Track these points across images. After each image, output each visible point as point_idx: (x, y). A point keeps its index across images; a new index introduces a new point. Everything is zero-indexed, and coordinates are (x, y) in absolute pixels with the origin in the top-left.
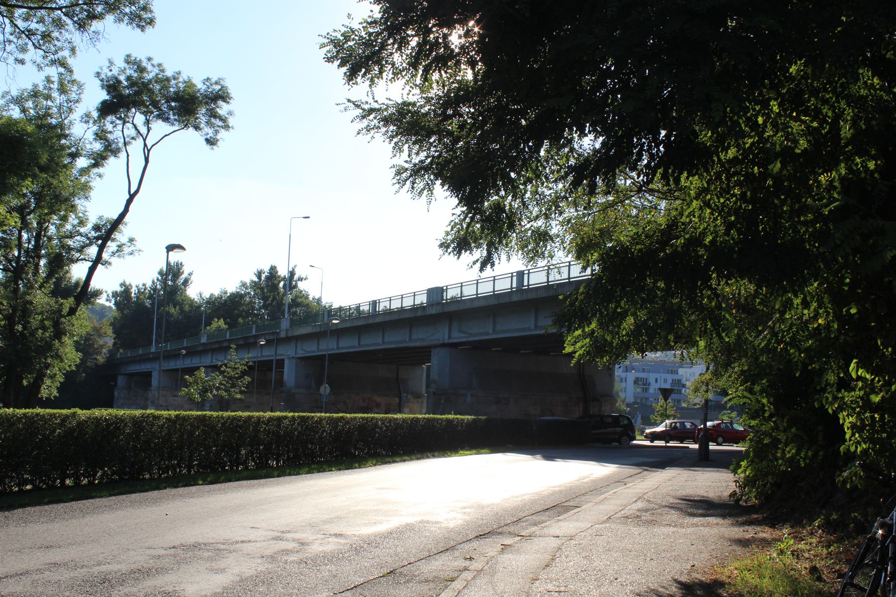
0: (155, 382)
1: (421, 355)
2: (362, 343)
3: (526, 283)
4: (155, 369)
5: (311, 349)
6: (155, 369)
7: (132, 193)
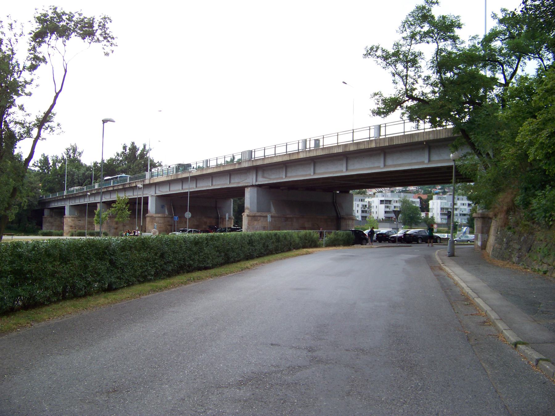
1: (239, 192)
2: (171, 189)
3: (253, 157)
4: (67, 205)
5: (165, 191)
6: (67, 205)
7: (57, 92)
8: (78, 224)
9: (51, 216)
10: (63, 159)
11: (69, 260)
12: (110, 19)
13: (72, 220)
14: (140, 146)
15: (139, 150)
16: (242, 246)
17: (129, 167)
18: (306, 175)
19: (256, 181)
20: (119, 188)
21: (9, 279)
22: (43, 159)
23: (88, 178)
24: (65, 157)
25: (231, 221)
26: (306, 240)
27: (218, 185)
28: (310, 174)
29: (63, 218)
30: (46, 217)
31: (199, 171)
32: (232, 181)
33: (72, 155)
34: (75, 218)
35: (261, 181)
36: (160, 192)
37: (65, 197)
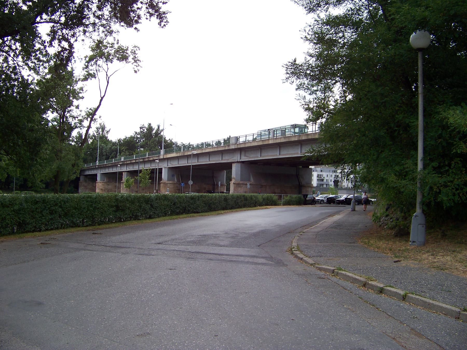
0: (99, 178)
1: (228, 166)
4: (99, 173)
5: (175, 164)
6: (99, 173)
7: (102, 97)
8: (107, 187)
9: (86, 181)
10: (94, 136)
11: (134, 203)
12: (139, 48)
13: (103, 185)
14: (155, 127)
15: (154, 130)
16: (220, 202)
17: (147, 144)
18: (274, 156)
19: (240, 159)
21: (114, 209)
22: (78, 135)
23: (114, 152)
24: (95, 134)
25: (224, 187)
26: (268, 200)
27: (214, 161)
28: (277, 155)
29: (94, 183)
30: (81, 182)
31: (200, 151)
32: (224, 158)
33: (101, 133)
34: (104, 183)
35: (244, 159)
37: (97, 167)
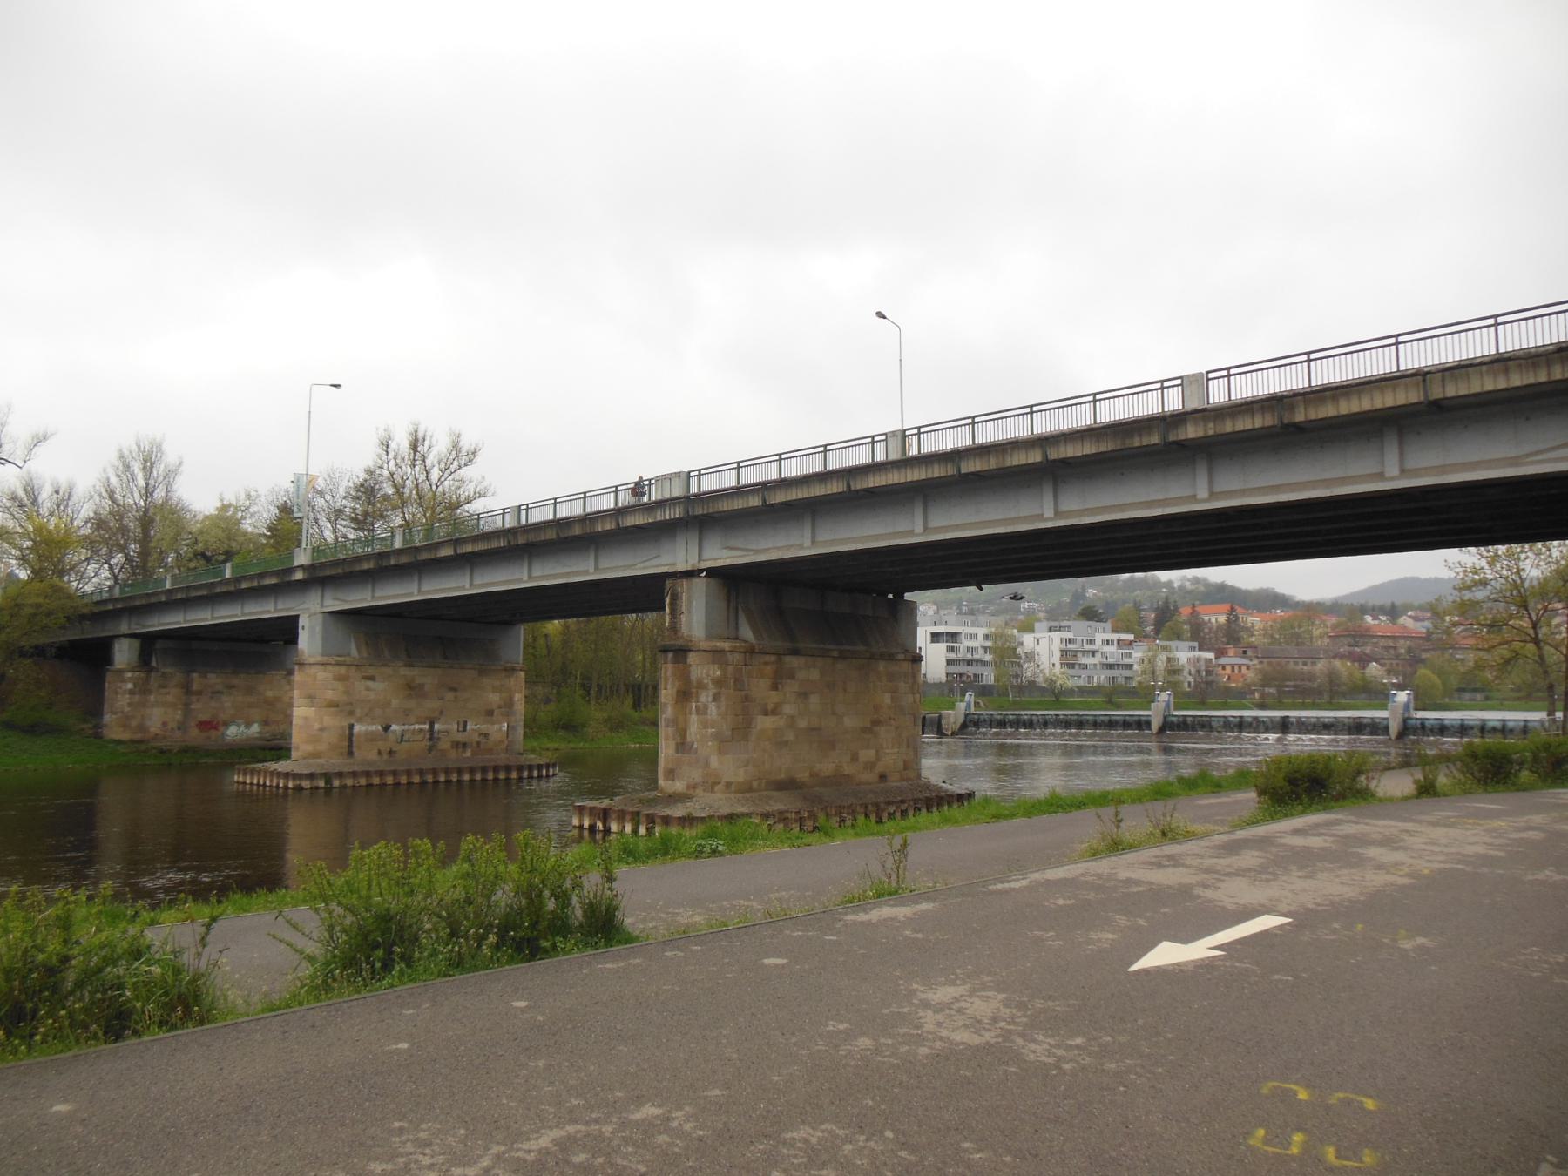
20: (459, 551)
36: (337, 602)
